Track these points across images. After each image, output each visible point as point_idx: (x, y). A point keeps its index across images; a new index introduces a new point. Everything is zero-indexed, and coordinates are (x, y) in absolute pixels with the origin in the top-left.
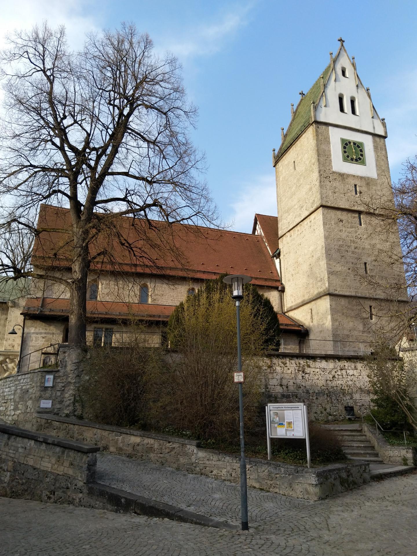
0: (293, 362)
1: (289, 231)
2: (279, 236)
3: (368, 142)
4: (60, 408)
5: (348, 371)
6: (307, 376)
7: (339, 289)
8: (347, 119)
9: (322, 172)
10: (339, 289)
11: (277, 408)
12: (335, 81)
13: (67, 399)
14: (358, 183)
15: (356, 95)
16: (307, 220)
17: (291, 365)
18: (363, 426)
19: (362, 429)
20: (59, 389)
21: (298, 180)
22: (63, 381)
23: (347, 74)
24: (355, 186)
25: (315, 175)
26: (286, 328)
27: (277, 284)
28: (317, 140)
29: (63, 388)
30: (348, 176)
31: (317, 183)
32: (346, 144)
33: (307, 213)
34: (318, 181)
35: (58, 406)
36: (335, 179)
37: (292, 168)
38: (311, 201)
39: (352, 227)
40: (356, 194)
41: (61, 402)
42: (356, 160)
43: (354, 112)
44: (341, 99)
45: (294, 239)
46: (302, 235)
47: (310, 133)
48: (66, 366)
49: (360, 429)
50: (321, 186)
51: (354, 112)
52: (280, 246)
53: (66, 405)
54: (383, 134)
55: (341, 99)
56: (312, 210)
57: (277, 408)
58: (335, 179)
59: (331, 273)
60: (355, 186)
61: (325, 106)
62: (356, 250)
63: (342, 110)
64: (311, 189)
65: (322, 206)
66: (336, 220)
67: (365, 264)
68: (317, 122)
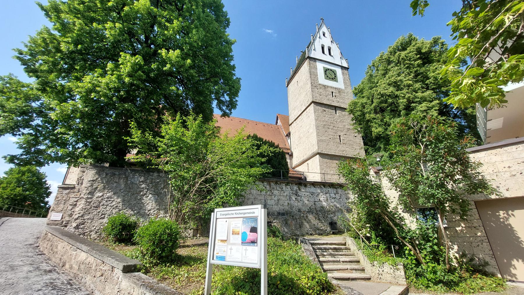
0: (288, 187)
1: (295, 120)
2: (290, 123)
3: (339, 71)
4: (69, 221)
5: (331, 195)
6: (299, 198)
7: (324, 150)
8: (327, 58)
9: (312, 84)
10: (324, 150)
11: (226, 215)
12: (319, 38)
13: (77, 213)
14: (334, 91)
15: (331, 46)
16: (305, 111)
17: (287, 190)
18: (347, 240)
19: (346, 243)
20: (71, 204)
21: (300, 91)
22: (77, 196)
23: (326, 35)
24: (332, 92)
25: (309, 85)
26: (293, 175)
27: (289, 151)
28: (310, 66)
29: (75, 203)
30: (328, 87)
31: (310, 90)
32: (326, 70)
33: (305, 108)
34: (311, 88)
35: (67, 218)
36: (321, 88)
37: (296, 85)
38: (307, 101)
39: (331, 115)
40: (333, 97)
41: (71, 215)
42: (332, 79)
43: (330, 54)
44: (323, 48)
45: (298, 124)
46: (302, 121)
47: (305, 67)
48: (82, 184)
49: (343, 242)
50: (312, 91)
51: (330, 54)
52: (290, 130)
53: (74, 218)
54: (347, 66)
55: (323, 48)
56: (307, 105)
57: (226, 215)
58: (321, 88)
59: (319, 141)
60: (332, 92)
61: (314, 50)
62: (334, 128)
63: (323, 52)
64: (307, 94)
65: (313, 102)
66: (322, 110)
67: (340, 136)
68: (309, 58)
